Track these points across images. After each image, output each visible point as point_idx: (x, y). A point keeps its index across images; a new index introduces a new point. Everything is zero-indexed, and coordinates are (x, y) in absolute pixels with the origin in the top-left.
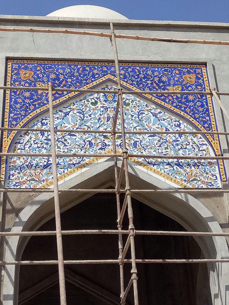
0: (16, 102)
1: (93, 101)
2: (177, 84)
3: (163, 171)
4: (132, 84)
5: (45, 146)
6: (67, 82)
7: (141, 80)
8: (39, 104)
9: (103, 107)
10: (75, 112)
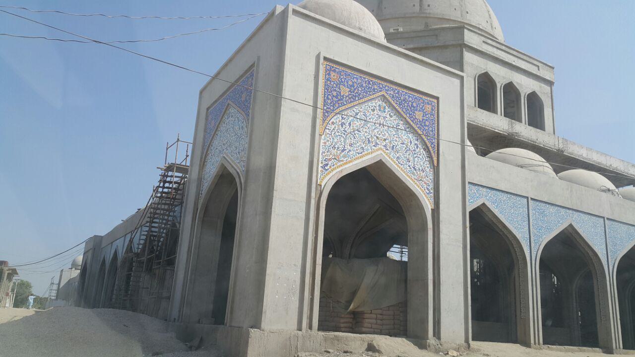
0: (409, 97)
1: (372, 108)
2: (421, 111)
3: (405, 170)
4: (396, 104)
5: (343, 136)
6: (358, 90)
7: (402, 102)
8: (341, 103)
9: (378, 114)
10: (362, 114)
